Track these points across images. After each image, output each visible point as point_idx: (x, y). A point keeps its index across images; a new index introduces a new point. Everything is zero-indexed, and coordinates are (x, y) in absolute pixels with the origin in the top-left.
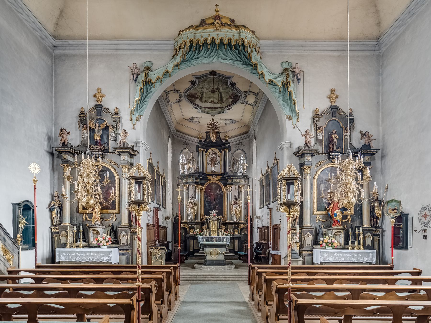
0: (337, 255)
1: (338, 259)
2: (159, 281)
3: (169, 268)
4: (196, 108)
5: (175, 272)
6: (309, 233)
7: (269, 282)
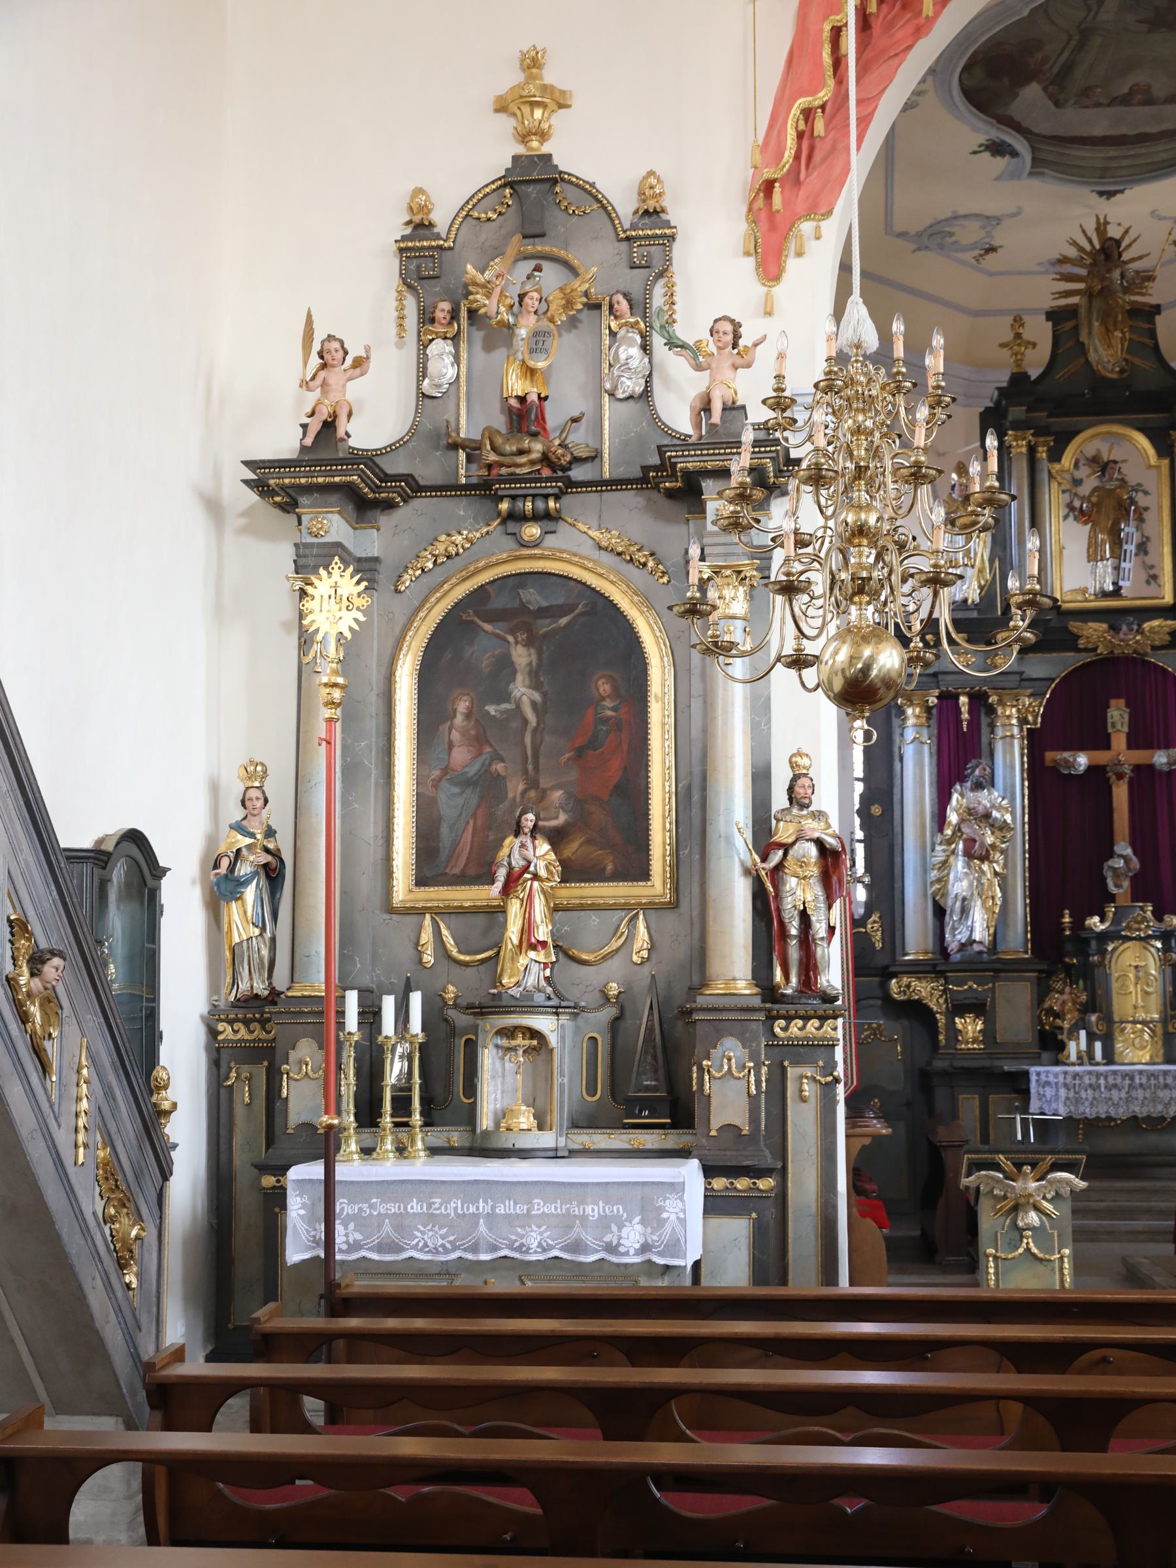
4: (997, 149)
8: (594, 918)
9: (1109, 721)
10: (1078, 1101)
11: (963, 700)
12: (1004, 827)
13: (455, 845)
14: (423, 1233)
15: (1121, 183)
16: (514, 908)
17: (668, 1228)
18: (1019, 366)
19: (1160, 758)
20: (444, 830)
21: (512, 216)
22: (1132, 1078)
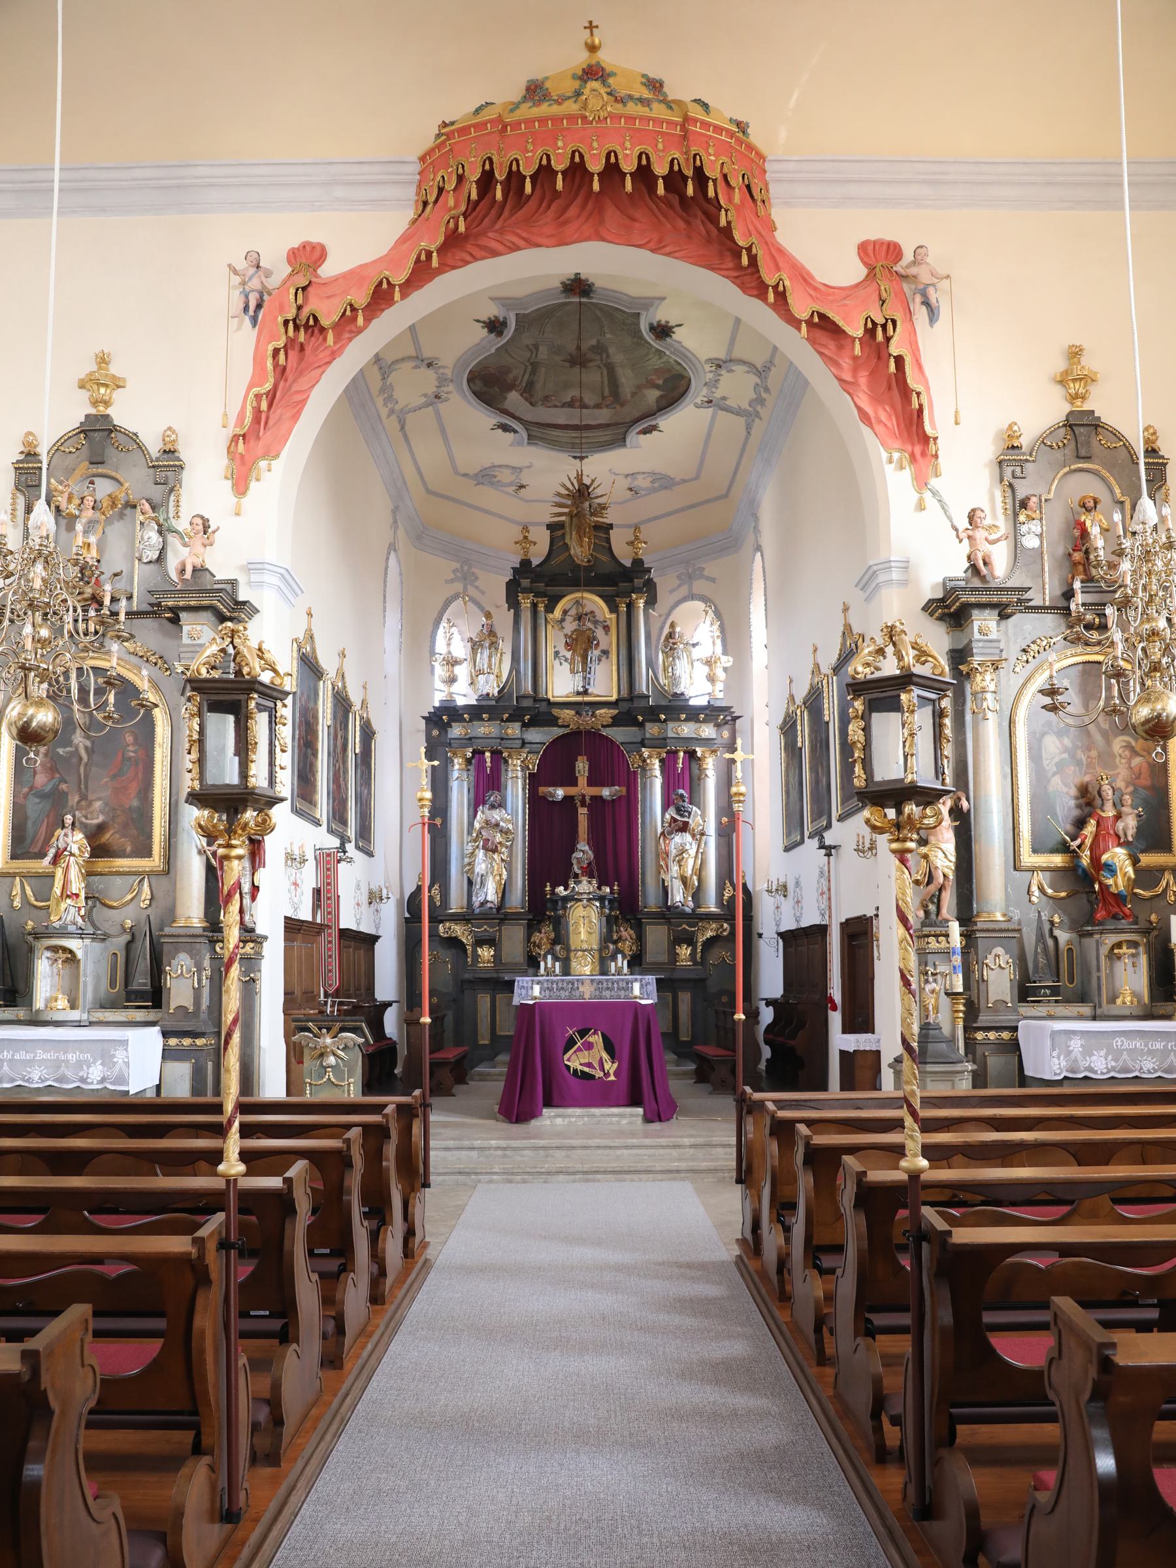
0: (1128, 1044)
1: (1130, 1064)
2: (329, 1165)
3: (378, 1109)
4: (505, 428)
5: (406, 1132)
6: (999, 950)
7: (823, 1162)
8: (118, 880)
11: (488, 754)
12: (505, 832)
13: (36, 834)
16: (59, 873)
17: (117, 1068)
19: (606, 792)
20: (29, 824)
21: (85, 451)
22: (573, 984)
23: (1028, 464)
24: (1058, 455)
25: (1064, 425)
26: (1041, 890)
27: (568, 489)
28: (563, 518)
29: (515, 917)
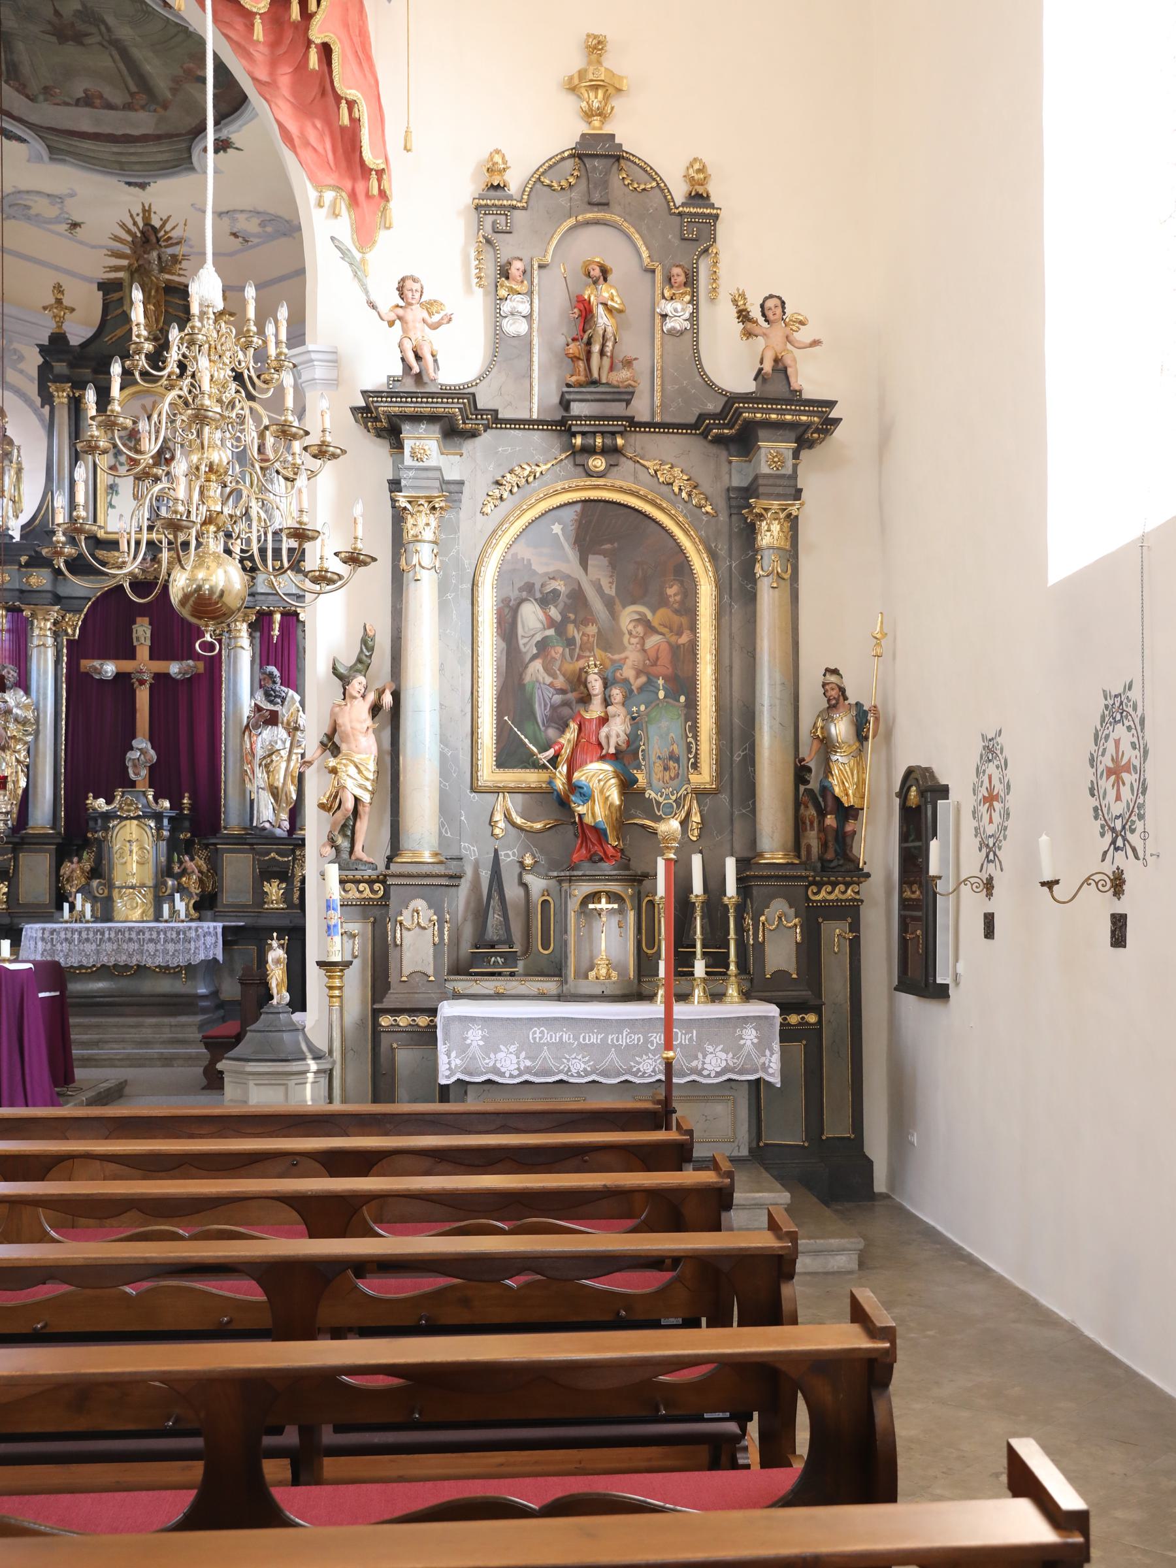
1: (552, 1063)
6: (419, 904)
9: (134, 635)
10: (53, 952)
14: (568, 1060)
15: (149, 176)
18: (60, 327)
22: (103, 934)
23: (516, 212)
24: (563, 200)
25: (572, 156)
26: (508, 818)
27: (129, 232)
28: (121, 275)
29: (38, 842)
